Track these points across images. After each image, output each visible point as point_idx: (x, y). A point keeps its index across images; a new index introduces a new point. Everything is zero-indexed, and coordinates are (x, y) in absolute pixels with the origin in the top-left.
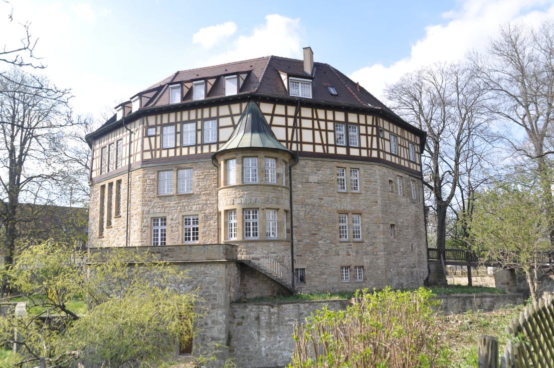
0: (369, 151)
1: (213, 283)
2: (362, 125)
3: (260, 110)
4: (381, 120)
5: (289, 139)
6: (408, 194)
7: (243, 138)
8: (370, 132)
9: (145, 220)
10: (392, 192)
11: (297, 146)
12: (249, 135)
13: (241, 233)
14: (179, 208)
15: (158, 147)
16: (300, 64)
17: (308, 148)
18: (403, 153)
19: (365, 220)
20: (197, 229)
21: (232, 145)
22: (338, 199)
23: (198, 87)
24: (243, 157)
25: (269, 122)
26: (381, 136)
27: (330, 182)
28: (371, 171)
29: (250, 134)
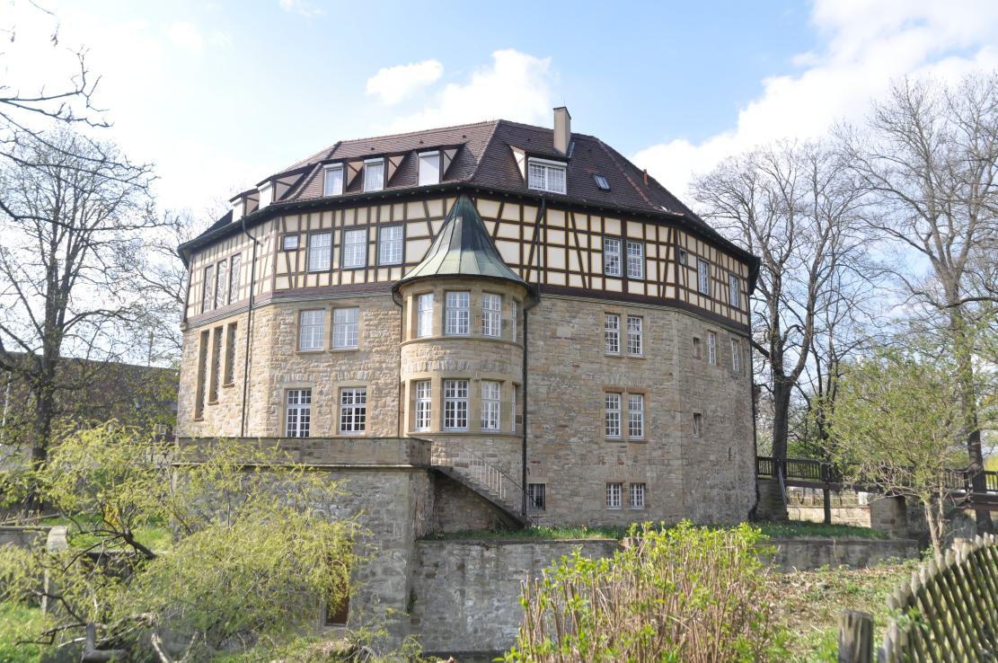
0: (662, 287)
4: (683, 235)
5: (526, 262)
6: (724, 363)
7: (446, 259)
8: (663, 255)
9: (275, 393)
10: (699, 358)
11: (539, 274)
12: (456, 253)
13: (438, 420)
14: (334, 374)
15: (302, 269)
16: (548, 135)
17: (556, 279)
19: (652, 405)
22: (605, 368)
24: (446, 291)
25: (491, 232)
26: (683, 261)
29: (458, 252)
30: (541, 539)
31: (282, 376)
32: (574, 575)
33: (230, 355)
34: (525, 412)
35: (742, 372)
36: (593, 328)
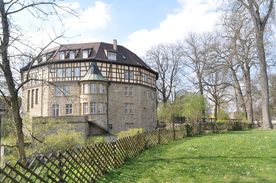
1: (81, 129)
2: (135, 71)
4: (142, 69)
5: (108, 76)
6: (151, 97)
7: (90, 76)
8: (137, 74)
9: (50, 106)
10: (145, 96)
12: (93, 75)
13: (89, 111)
14: (64, 101)
16: (111, 46)
17: (114, 80)
18: (149, 81)
19: (135, 106)
20: (71, 109)
21: (86, 78)
22: (125, 99)
23: (72, 54)
24: (91, 83)
25: (100, 70)
26: (141, 75)
29: (93, 75)
30: (112, 135)
32: (243, 31)
33: (37, 96)
34: (108, 109)
35: (154, 98)
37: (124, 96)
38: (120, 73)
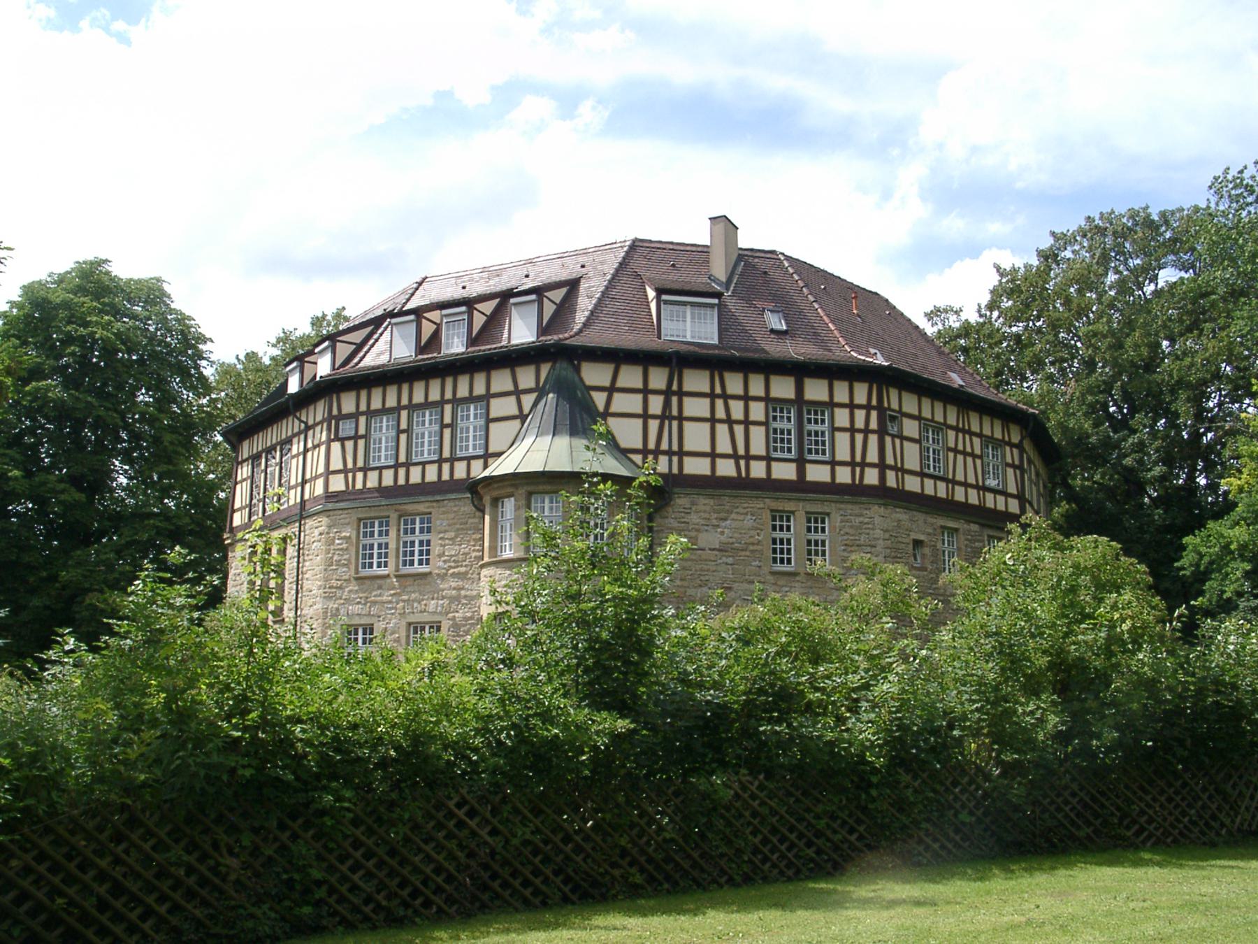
0: (858, 470)
3: (581, 380)
5: (652, 445)
8: (860, 424)
11: (670, 461)
15: (360, 464)
17: (696, 467)
25: (601, 408)
27: (751, 548)
28: (861, 519)
31: (337, 609)
36: (753, 533)
37: (766, 570)
38: (721, 421)
